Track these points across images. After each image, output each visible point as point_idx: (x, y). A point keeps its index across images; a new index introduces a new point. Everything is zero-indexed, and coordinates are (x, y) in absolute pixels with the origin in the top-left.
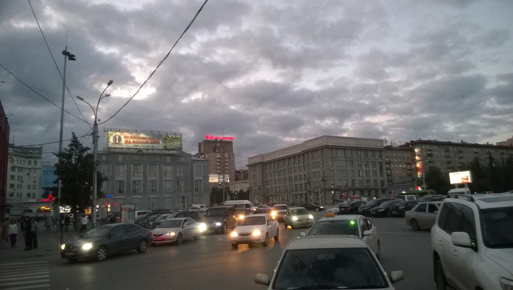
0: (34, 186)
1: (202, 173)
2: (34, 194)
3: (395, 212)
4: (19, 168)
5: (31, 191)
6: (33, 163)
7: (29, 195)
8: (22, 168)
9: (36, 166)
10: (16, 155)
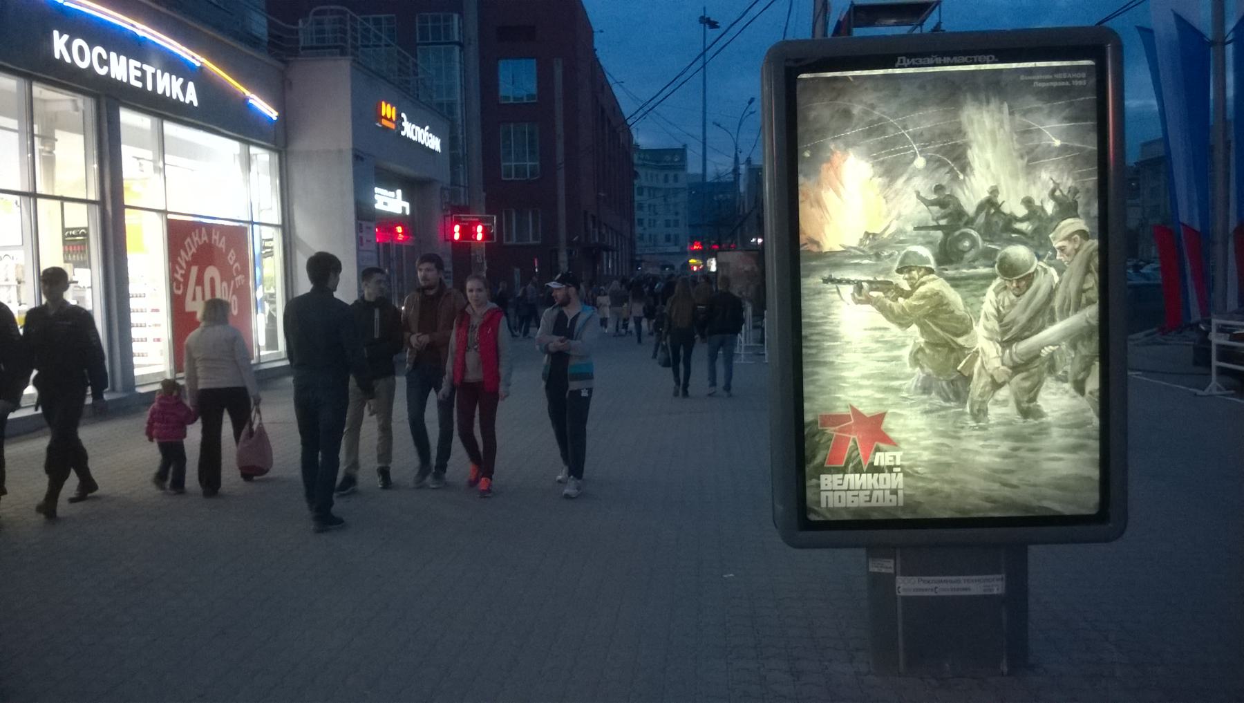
0: (677, 222)
1: (563, 257)
2: (677, 237)
3: (479, 237)
4: (650, 188)
5: (672, 231)
6: (671, 178)
7: (668, 238)
8: (655, 189)
9: (678, 185)
10: (644, 165)
